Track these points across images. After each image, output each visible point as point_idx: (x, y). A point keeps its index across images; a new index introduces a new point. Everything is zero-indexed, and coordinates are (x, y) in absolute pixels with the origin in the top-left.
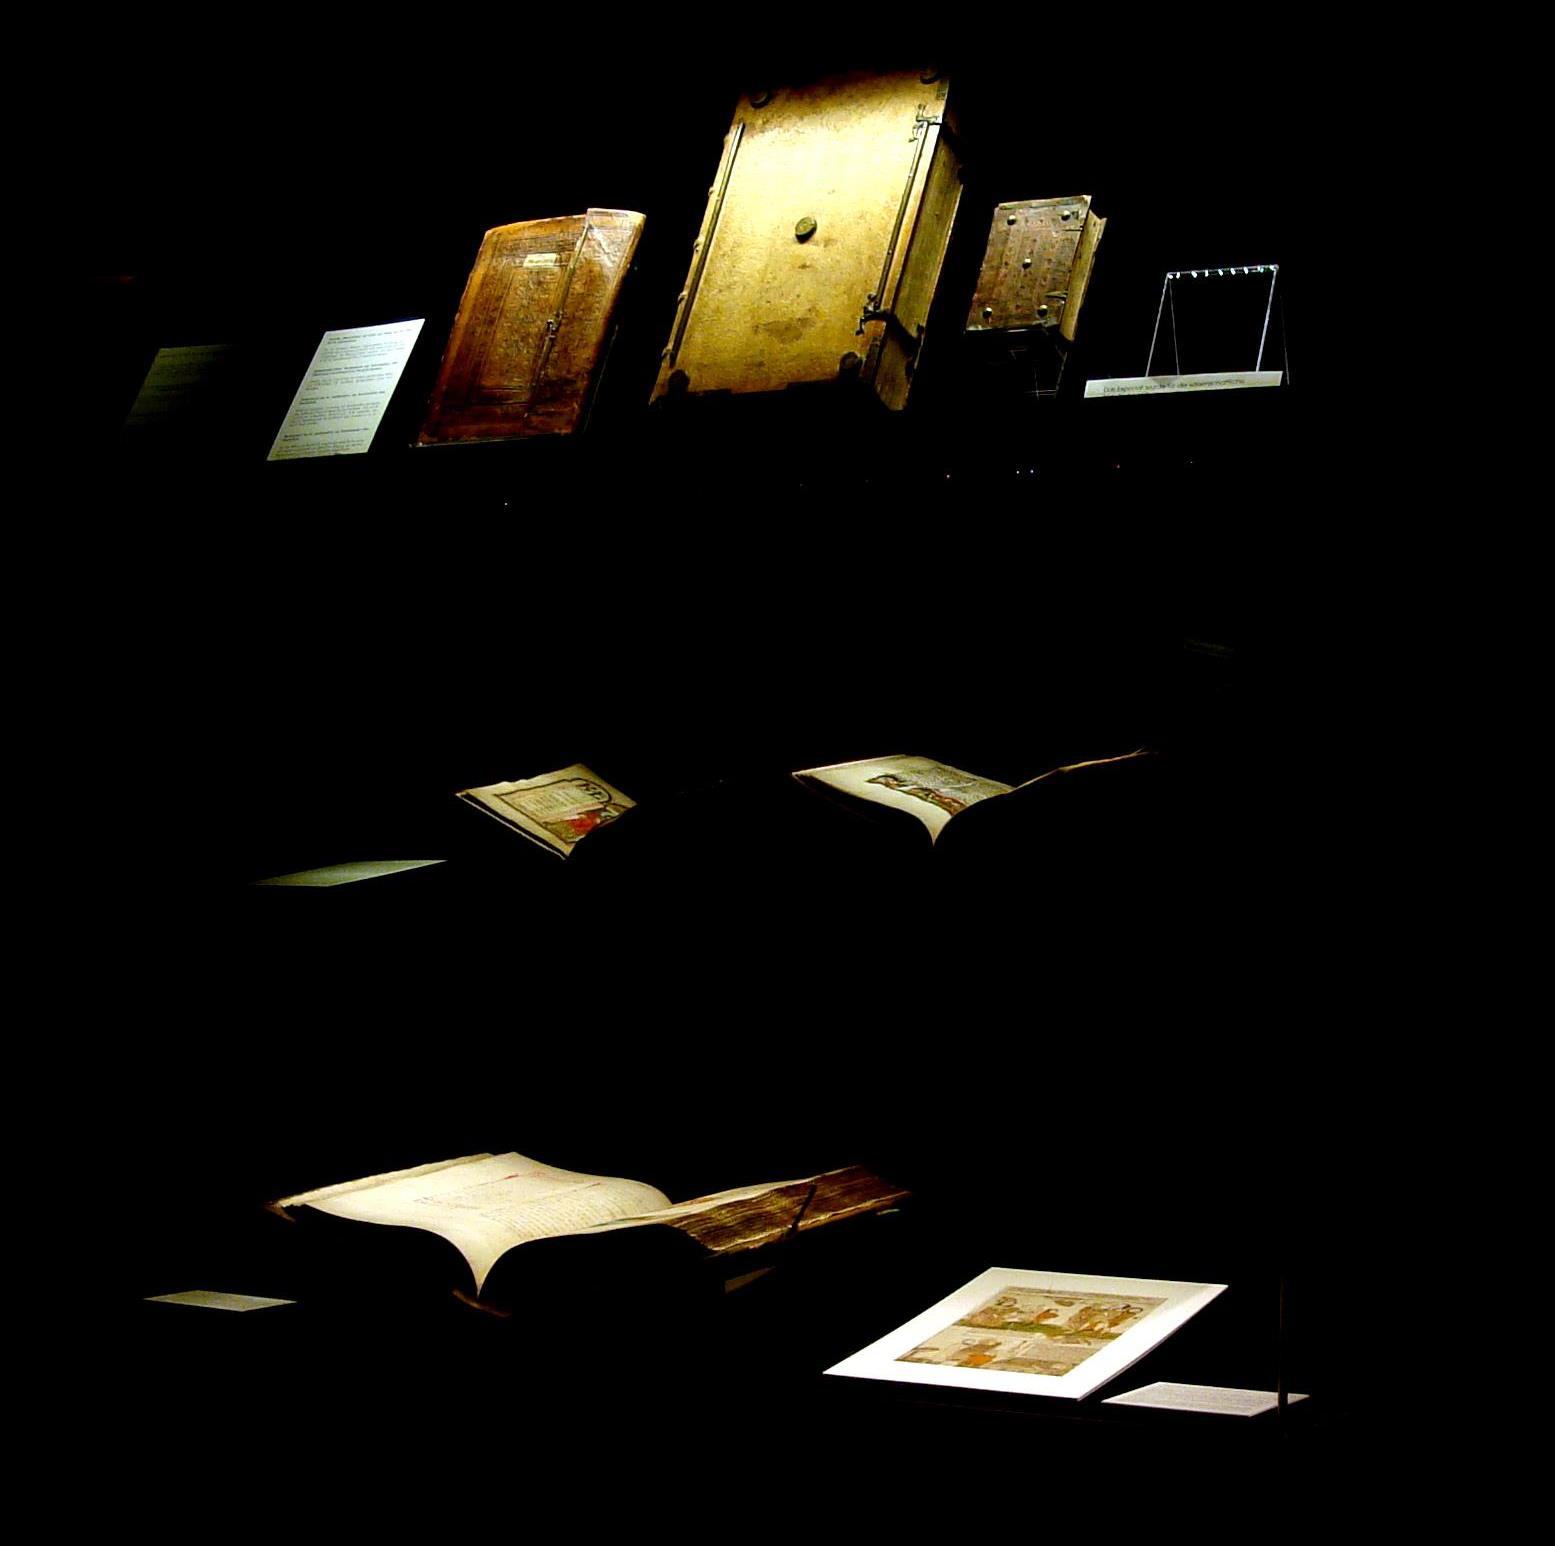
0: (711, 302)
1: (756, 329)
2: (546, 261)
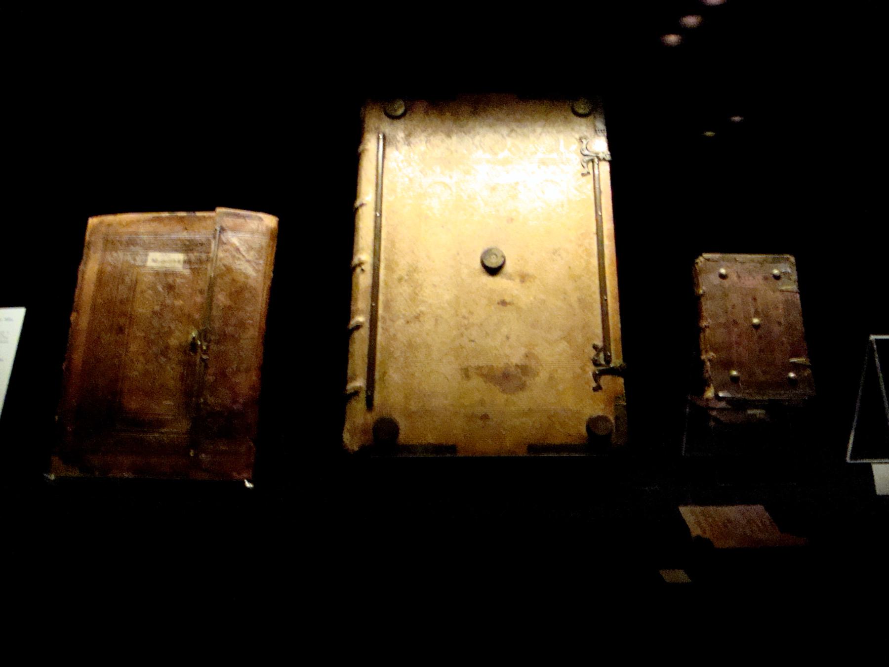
0: (399, 335)
1: (466, 373)
2: (170, 261)
